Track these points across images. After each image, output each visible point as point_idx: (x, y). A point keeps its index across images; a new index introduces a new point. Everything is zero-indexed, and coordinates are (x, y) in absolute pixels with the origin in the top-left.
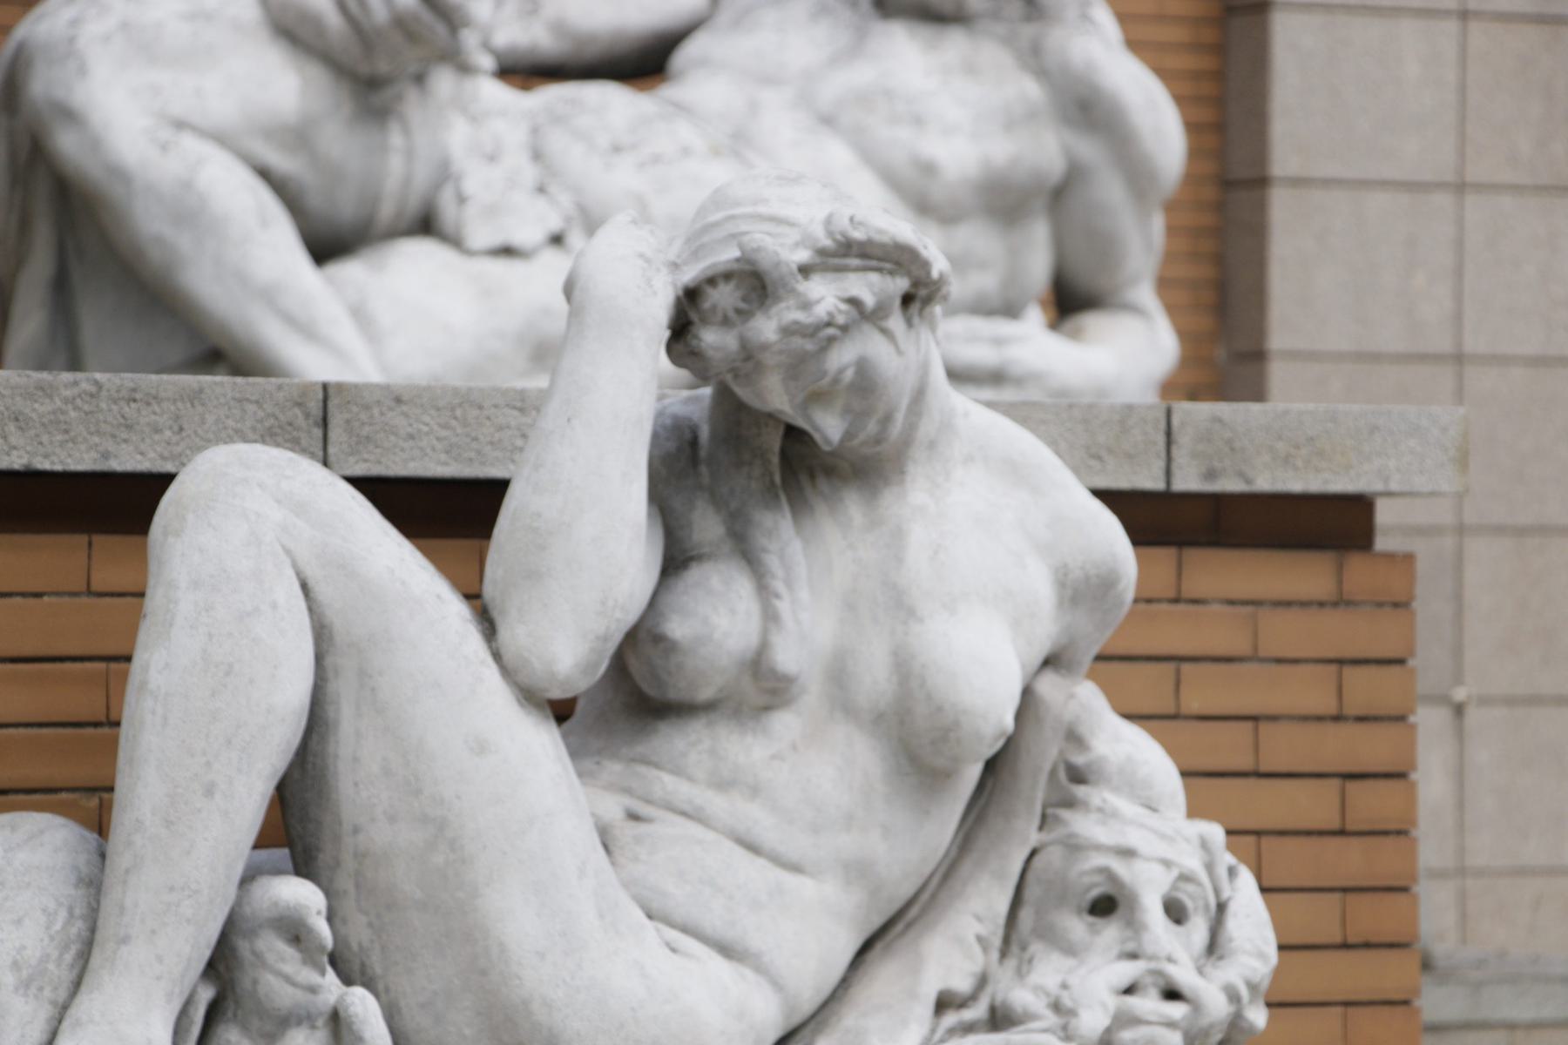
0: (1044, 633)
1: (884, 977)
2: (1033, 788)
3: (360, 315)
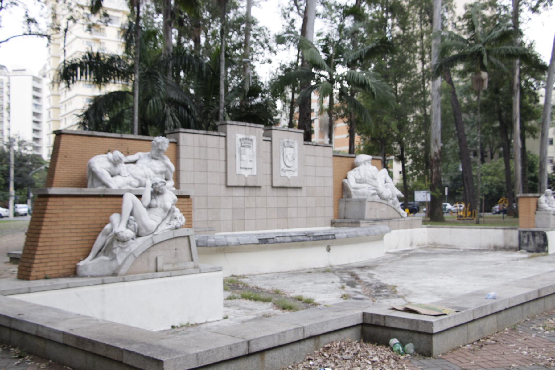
0: (172, 203)
1: (163, 223)
2: (171, 211)
3: (115, 181)
